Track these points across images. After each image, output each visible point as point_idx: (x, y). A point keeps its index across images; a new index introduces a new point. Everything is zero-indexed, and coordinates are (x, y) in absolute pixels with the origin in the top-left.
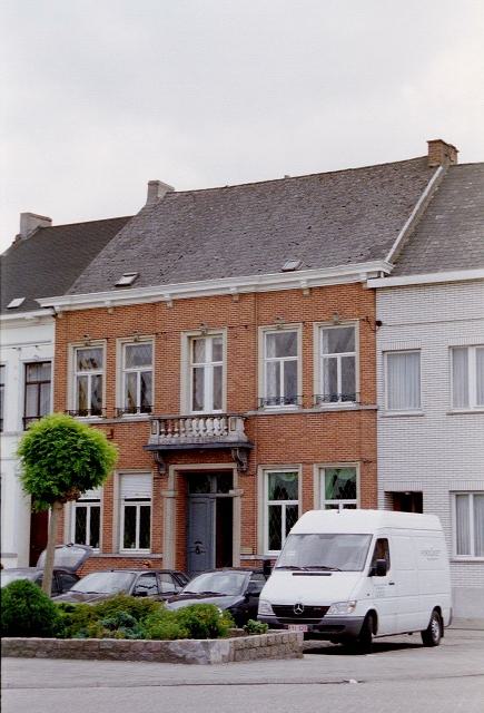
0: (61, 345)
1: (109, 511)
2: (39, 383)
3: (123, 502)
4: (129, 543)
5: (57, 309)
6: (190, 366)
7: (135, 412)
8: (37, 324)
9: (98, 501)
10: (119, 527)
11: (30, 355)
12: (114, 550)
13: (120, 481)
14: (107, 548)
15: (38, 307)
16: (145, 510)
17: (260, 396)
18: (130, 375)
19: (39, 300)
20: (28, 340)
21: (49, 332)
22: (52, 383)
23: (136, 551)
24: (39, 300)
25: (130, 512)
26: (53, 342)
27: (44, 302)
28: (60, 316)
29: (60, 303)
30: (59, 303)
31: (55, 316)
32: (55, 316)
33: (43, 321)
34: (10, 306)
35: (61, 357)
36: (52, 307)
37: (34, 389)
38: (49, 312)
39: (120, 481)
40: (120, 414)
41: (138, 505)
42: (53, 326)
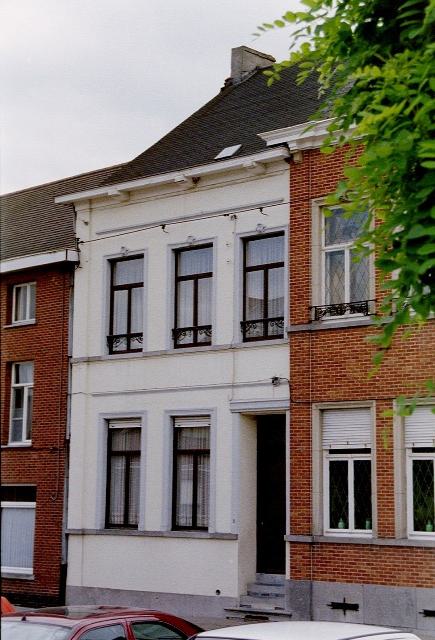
0: (299, 203)
1: (386, 468)
2: (266, 268)
3: (326, 454)
4: (338, 516)
5: (293, 146)
6: (321, 250)
7: (342, 313)
8: (260, 176)
9: (367, 451)
10: (404, 494)
11: (249, 224)
12: (398, 533)
13: (322, 419)
14: (387, 529)
15: (262, 146)
16: (363, 469)
17: (315, 303)
18: (331, 255)
19: (263, 136)
20: (245, 203)
21: (279, 186)
22: (286, 264)
23: (350, 533)
24: (263, 136)
25: (338, 470)
26: (287, 199)
27: (271, 137)
28: (297, 158)
29: (297, 137)
30: (294, 136)
31: (289, 160)
32: (289, 160)
33: (136, 198)
34: (218, 157)
35: (300, 225)
36: (285, 145)
37: (187, 287)
38: (280, 152)
39: (322, 419)
40: (319, 314)
41: (351, 459)
42: (287, 175)
